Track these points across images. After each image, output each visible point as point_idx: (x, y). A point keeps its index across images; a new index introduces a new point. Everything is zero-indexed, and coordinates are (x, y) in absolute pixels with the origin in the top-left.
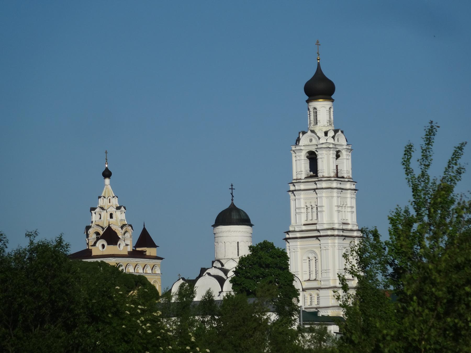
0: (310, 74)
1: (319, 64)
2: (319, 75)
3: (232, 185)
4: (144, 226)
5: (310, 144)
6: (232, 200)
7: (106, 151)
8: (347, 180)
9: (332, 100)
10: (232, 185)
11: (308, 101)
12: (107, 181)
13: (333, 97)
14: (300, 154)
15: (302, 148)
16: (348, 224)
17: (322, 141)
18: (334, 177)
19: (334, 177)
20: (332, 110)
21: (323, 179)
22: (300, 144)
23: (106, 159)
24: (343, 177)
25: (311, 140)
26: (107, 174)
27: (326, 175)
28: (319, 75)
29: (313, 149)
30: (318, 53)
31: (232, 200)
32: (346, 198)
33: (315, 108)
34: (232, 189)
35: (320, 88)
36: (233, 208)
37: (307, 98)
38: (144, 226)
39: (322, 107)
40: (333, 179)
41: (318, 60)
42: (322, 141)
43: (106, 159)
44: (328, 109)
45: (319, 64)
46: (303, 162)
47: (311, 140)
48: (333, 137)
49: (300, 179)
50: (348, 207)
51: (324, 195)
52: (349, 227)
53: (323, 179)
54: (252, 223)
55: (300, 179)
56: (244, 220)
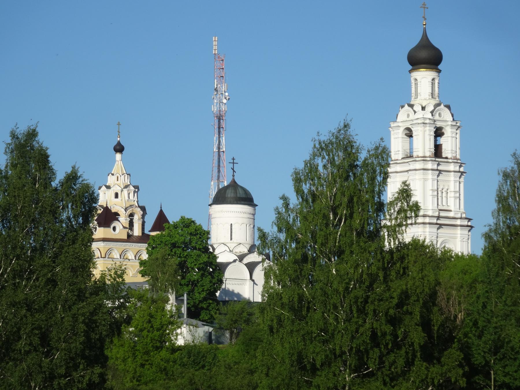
0: (415, 40)
1: (425, 30)
2: (425, 44)
3: (233, 159)
4: (161, 208)
5: (408, 119)
6: (233, 176)
7: (119, 123)
8: (450, 161)
9: (439, 71)
10: (233, 159)
11: (410, 71)
12: (118, 156)
13: (440, 67)
14: (397, 131)
15: (400, 124)
16: (450, 211)
17: (418, 116)
18: (430, 157)
19: (430, 157)
20: (437, 81)
21: (417, 159)
22: (398, 120)
23: (119, 132)
24: (446, 158)
25: (408, 116)
26: (119, 149)
27: (421, 154)
28: (425, 44)
29: (408, 125)
30: (424, 17)
31: (233, 176)
32: (449, 181)
33: (416, 80)
34: (233, 163)
35: (426, 57)
36: (234, 185)
37: (410, 67)
38: (161, 208)
39: (424, 77)
40: (428, 159)
41: (424, 25)
42: (418, 116)
43: (119, 132)
44: (430, 80)
45: (425, 30)
46: (400, 140)
47: (408, 116)
48: (432, 112)
49: (397, 160)
50: (450, 192)
51: (417, 177)
52: (451, 214)
53: (417, 159)
54: (255, 202)
55: (397, 160)
56: (247, 199)
